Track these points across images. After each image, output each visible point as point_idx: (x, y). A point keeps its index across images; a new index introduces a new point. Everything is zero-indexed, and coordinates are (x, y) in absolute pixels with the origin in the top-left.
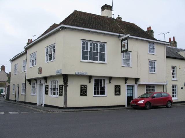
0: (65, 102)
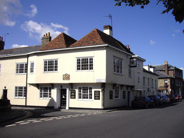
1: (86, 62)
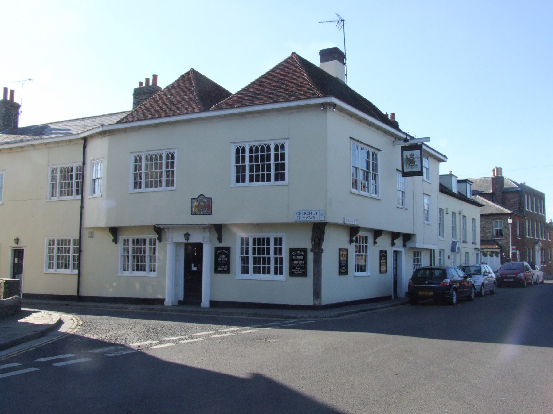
0: (317, 293)
1: (262, 156)
